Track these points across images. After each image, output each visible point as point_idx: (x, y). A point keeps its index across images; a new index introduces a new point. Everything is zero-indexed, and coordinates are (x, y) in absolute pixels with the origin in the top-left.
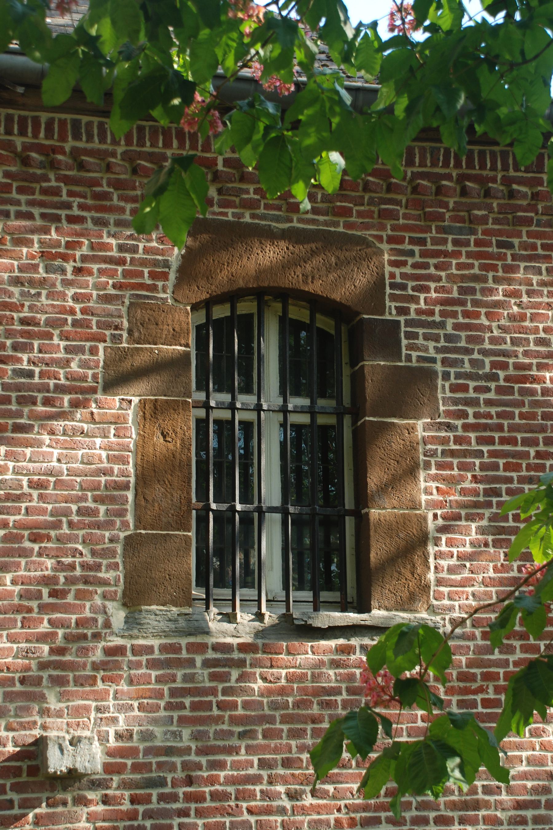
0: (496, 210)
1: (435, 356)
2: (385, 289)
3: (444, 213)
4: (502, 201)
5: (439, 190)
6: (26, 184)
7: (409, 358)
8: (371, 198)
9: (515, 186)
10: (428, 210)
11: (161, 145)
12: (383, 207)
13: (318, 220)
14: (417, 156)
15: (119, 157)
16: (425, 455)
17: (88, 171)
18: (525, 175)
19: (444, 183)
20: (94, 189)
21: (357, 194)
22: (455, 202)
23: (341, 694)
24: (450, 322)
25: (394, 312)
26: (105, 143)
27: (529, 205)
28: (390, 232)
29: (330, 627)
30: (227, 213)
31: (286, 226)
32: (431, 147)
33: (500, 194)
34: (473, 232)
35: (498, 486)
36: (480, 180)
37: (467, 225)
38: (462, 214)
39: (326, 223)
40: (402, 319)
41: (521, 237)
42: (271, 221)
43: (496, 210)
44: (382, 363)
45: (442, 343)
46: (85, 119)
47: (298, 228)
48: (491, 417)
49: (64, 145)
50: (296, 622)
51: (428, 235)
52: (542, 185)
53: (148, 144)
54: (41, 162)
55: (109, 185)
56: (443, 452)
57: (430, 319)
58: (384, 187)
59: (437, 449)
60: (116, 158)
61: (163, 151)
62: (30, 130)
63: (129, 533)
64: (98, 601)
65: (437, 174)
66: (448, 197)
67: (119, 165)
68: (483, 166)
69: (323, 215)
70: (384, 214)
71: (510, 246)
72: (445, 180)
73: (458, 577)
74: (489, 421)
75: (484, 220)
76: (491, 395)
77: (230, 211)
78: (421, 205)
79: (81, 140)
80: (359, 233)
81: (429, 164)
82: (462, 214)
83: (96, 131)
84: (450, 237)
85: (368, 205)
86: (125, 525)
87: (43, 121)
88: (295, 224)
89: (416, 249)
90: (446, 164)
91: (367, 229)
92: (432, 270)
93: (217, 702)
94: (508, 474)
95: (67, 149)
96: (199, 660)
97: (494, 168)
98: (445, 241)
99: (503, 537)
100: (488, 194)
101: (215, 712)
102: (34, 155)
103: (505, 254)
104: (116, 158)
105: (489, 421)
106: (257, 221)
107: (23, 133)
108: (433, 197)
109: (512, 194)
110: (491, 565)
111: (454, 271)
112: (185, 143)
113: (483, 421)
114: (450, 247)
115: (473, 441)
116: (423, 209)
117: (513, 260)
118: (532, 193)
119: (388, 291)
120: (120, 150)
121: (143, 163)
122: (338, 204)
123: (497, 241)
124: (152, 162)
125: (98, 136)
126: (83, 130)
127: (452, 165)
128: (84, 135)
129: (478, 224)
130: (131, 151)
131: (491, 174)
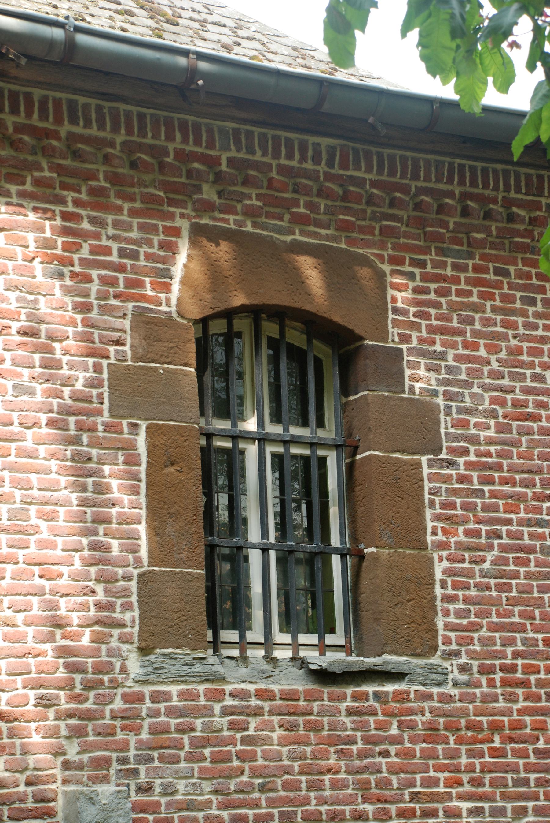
0: (494, 233)
1: (436, 388)
2: (387, 313)
3: (444, 233)
4: (500, 225)
5: (441, 209)
6: (16, 171)
7: (412, 388)
8: (373, 213)
9: (515, 209)
10: (428, 229)
11: (163, 138)
12: (385, 223)
13: (320, 234)
14: (422, 169)
15: (118, 147)
16: (430, 494)
17: (84, 162)
18: (525, 197)
19: (448, 201)
20: (90, 183)
21: (360, 207)
22: (455, 223)
23: (356, 743)
24: (451, 354)
25: (397, 339)
26: (104, 130)
27: (525, 230)
28: (390, 252)
29: (344, 672)
30: (228, 220)
31: (289, 238)
32: (436, 161)
33: (500, 217)
34: (471, 256)
35: (499, 528)
36: (482, 200)
37: (465, 248)
38: (460, 235)
39: (328, 238)
40: (404, 347)
41: (516, 265)
42: (273, 231)
43: (494, 233)
44: (386, 394)
45: (444, 375)
46: (82, 100)
47: (300, 241)
48: (491, 456)
49: (59, 129)
50: (312, 667)
51: (427, 257)
52: (540, 209)
53: (150, 135)
54: (33, 147)
55: (106, 180)
56: (447, 490)
57: (431, 348)
58: (387, 201)
59: (441, 487)
60: (115, 148)
61: (165, 144)
62: (22, 108)
63: (142, 570)
64: (114, 643)
65: (440, 190)
66: (449, 216)
67: (117, 157)
68: (486, 186)
69: (324, 228)
70: (386, 232)
71: (507, 274)
72: (448, 197)
73: (465, 622)
74: (489, 460)
75: (482, 244)
76: (491, 433)
77: (231, 218)
78: (421, 223)
79: (78, 124)
80: (361, 251)
81: (434, 180)
82: (460, 235)
83: (94, 116)
84: (449, 260)
85: (370, 220)
86: (138, 562)
87: (36, 99)
88: (298, 237)
89: (417, 271)
90: (450, 181)
91: (369, 247)
92: (432, 296)
93: (236, 751)
94: (508, 516)
95: (63, 134)
96: (217, 708)
97: (496, 188)
98: (444, 265)
99: (504, 581)
100: (488, 215)
101: (236, 763)
102: (26, 138)
103: (502, 282)
104: (115, 148)
105: (489, 460)
106: (259, 231)
107: (15, 111)
108: (434, 216)
109: (511, 218)
110: (494, 609)
111: (454, 298)
112: (188, 138)
113: (484, 459)
114: (449, 272)
115: (475, 480)
116: (424, 228)
117: (509, 289)
118: (530, 218)
119: (391, 316)
120: (120, 139)
121: (143, 156)
122: (341, 217)
123: (494, 267)
124: (153, 157)
125: (96, 121)
126: (80, 114)
127: (456, 182)
128: (81, 119)
129: (477, 248)
130: (131, 141)
131: (493, 194)
